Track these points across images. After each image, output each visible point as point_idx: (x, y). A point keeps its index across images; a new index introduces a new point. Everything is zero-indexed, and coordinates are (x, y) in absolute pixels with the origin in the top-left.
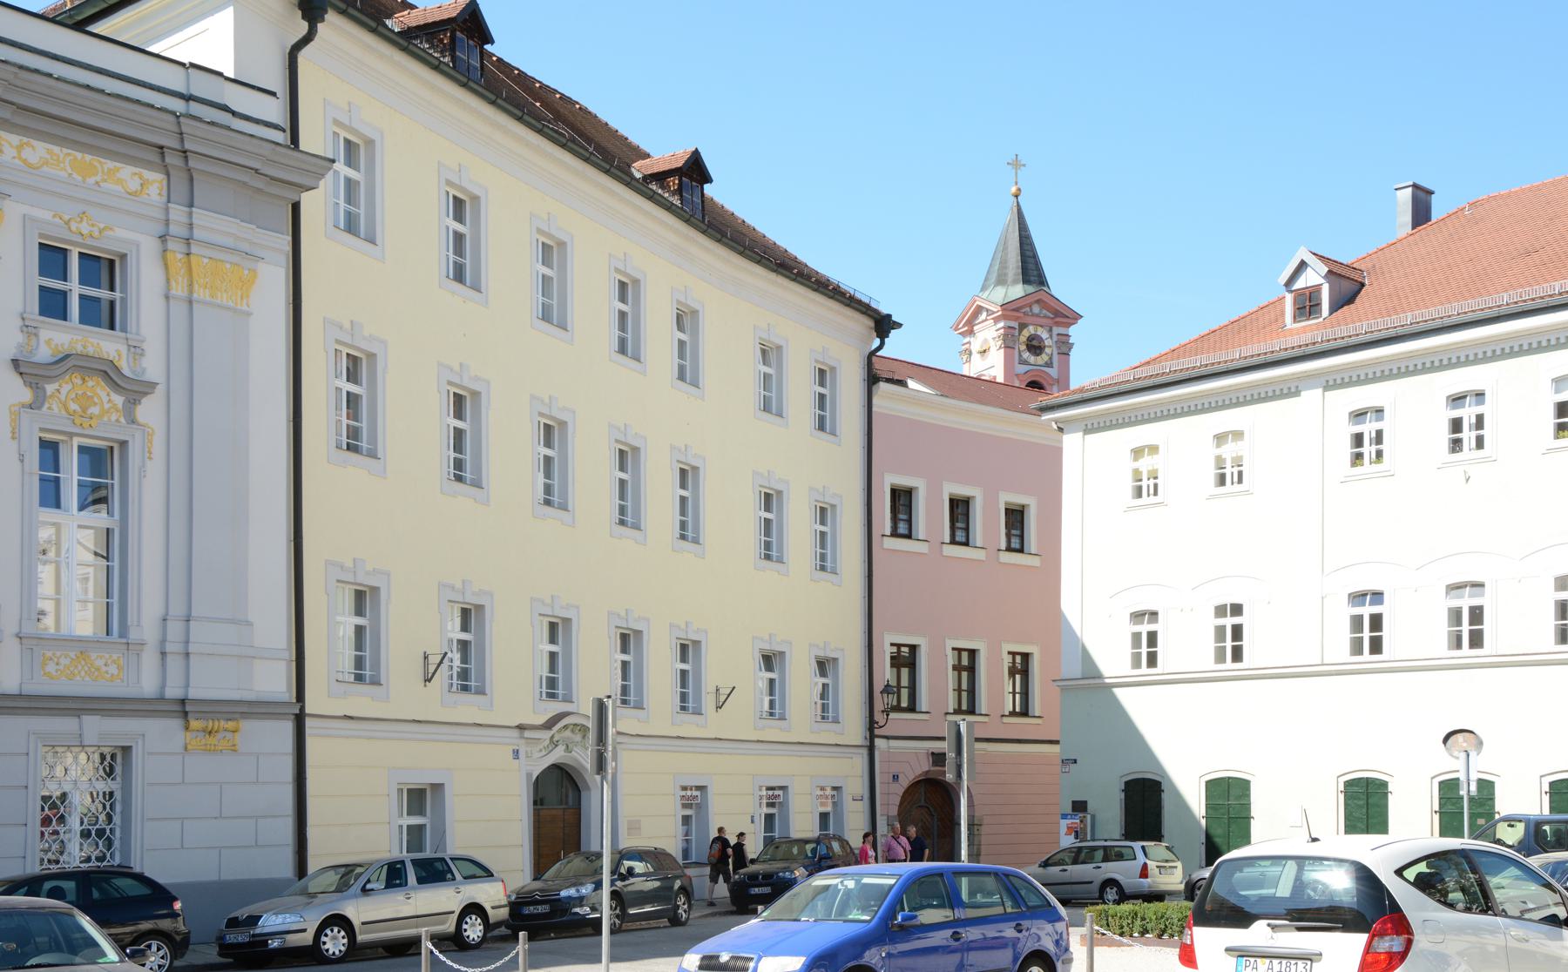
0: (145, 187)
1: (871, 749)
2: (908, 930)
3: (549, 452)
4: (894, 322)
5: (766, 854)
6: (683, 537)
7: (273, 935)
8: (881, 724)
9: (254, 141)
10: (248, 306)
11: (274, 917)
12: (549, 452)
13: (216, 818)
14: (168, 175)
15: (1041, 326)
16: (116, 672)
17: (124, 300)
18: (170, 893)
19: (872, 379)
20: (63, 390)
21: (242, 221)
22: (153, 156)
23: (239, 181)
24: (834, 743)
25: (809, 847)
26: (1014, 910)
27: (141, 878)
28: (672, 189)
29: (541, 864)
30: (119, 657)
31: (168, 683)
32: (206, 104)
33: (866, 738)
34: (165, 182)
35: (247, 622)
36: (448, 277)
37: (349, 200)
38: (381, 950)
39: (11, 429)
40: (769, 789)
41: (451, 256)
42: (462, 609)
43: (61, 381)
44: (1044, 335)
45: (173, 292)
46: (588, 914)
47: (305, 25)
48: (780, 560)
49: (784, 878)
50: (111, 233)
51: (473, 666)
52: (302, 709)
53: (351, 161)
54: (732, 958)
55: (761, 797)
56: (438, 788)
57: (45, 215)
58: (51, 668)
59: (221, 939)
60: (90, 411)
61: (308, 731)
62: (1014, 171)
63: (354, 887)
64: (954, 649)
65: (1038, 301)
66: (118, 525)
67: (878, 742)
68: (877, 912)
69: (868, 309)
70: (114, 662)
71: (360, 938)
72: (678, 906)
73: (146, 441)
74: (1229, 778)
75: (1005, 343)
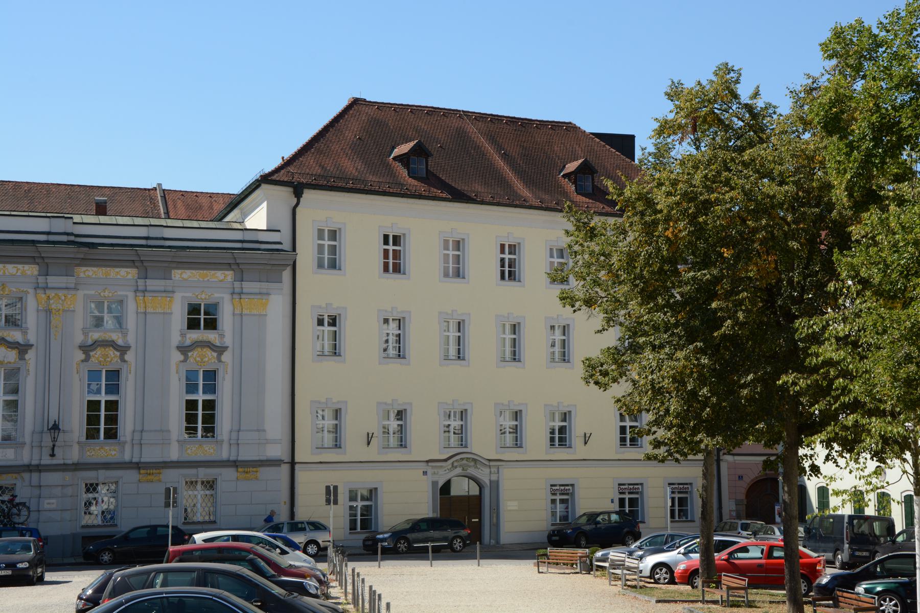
20: (194, 355)
45: (139, 311)
57: (93, 292)
58: (189, 451)
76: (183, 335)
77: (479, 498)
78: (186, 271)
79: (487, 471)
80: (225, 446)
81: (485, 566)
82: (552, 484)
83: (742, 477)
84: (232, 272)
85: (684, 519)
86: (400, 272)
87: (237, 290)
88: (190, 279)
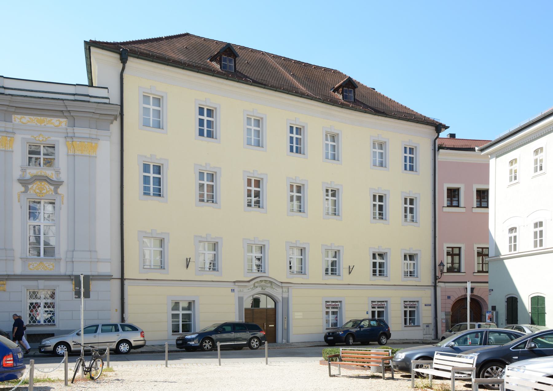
1: (435, 287)
9: (99, 104)
16: (52, 268)
20: (34, 187)
30: (53, 263)
33: (433, 283)
39: (18, 199)
43: (33, 184)
45: (69, 153)
50: (50, 139)
57: (29, 137)
58: (31, 267)
60: (42, 192)
70: (51, 264)
74: (538, 296)
76: (23, 170)
77: (275, 310)
78: (25, 116)
79: (280, 290)
80: (63, 264)
81: (274, 364)
82: (326, 300)
83: (450, 297)
84: (65, 120)
85: (412, 325)
86: (213, 138)
87: (70, 135)
88: (29, 123)
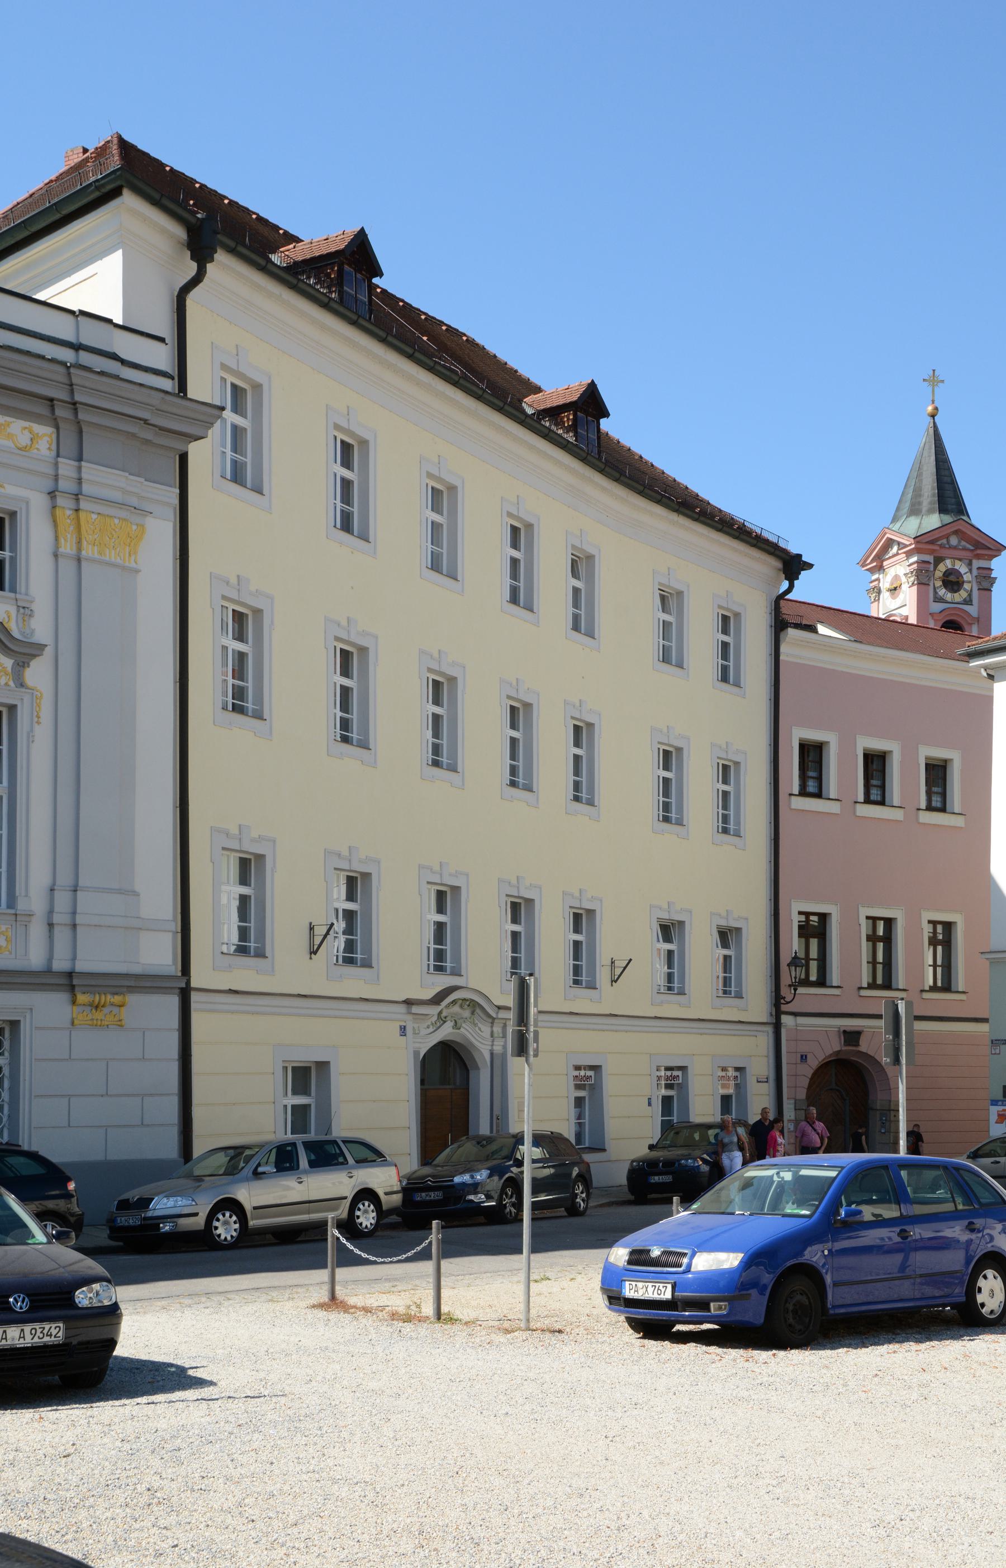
0: (34, 442)
1: (777, 1026)
2: (853, 1225)
3: (438, 710)
4: (805, 563)
5: (666, 1139)
6: (513, 784)
7: (165, 1218)
8: (788, 999)
9: (143, 390)
10: (136, 562)
11: (165, 1200)
12: (438, 710)
13: (102, 1096)
14: (58, 428)
15: (960, 560)
17: (13, 560)
18: (64, 1173)
19: (780, 625)
21: (146, 480)
22: (43, 410)
23: (128, 433)
24: (737, 1020)
25: (711, 1133)
26: (967, 1208)
27: (34, 1156)
28: (566, 425)
29: (428, 1151)
30: (7, 929)
31: (55, 957)
32: (95, 353)
33: (771, 1015)
34: (54, 436)
35: (135, 892)
36: (335, 526)
37: (235, 449)
38: (269, 1236)
40: (667, 1069)
41: (339, 504)
42: (241, 859)
44: (963, 569)
45: (62, 550)
46: (483, 1202)
47: (193, 267)
48: (680, 823)
49: (686, 1166)
51: (358, 938)
52: (188, 982)
53: (238, 408)
54: (664, 1253)
55: (659, 1078)
56: (323, 1066)
59: (111, 1221)
61: (193, 1006)
62: (930, 389)
63: (245, 1170)
64: (868, 918)
65: (956, 532)
66: (7, 792)
67: (785, 1019)
68: (818, 1207)
69: (775, 549)
71: (252, 1223)
72: (577, 1195)
73: (35, 704)
75: (918, 579)
83: (806, 1056)
